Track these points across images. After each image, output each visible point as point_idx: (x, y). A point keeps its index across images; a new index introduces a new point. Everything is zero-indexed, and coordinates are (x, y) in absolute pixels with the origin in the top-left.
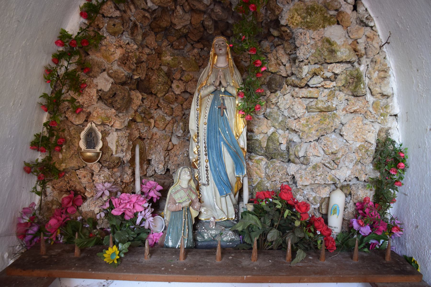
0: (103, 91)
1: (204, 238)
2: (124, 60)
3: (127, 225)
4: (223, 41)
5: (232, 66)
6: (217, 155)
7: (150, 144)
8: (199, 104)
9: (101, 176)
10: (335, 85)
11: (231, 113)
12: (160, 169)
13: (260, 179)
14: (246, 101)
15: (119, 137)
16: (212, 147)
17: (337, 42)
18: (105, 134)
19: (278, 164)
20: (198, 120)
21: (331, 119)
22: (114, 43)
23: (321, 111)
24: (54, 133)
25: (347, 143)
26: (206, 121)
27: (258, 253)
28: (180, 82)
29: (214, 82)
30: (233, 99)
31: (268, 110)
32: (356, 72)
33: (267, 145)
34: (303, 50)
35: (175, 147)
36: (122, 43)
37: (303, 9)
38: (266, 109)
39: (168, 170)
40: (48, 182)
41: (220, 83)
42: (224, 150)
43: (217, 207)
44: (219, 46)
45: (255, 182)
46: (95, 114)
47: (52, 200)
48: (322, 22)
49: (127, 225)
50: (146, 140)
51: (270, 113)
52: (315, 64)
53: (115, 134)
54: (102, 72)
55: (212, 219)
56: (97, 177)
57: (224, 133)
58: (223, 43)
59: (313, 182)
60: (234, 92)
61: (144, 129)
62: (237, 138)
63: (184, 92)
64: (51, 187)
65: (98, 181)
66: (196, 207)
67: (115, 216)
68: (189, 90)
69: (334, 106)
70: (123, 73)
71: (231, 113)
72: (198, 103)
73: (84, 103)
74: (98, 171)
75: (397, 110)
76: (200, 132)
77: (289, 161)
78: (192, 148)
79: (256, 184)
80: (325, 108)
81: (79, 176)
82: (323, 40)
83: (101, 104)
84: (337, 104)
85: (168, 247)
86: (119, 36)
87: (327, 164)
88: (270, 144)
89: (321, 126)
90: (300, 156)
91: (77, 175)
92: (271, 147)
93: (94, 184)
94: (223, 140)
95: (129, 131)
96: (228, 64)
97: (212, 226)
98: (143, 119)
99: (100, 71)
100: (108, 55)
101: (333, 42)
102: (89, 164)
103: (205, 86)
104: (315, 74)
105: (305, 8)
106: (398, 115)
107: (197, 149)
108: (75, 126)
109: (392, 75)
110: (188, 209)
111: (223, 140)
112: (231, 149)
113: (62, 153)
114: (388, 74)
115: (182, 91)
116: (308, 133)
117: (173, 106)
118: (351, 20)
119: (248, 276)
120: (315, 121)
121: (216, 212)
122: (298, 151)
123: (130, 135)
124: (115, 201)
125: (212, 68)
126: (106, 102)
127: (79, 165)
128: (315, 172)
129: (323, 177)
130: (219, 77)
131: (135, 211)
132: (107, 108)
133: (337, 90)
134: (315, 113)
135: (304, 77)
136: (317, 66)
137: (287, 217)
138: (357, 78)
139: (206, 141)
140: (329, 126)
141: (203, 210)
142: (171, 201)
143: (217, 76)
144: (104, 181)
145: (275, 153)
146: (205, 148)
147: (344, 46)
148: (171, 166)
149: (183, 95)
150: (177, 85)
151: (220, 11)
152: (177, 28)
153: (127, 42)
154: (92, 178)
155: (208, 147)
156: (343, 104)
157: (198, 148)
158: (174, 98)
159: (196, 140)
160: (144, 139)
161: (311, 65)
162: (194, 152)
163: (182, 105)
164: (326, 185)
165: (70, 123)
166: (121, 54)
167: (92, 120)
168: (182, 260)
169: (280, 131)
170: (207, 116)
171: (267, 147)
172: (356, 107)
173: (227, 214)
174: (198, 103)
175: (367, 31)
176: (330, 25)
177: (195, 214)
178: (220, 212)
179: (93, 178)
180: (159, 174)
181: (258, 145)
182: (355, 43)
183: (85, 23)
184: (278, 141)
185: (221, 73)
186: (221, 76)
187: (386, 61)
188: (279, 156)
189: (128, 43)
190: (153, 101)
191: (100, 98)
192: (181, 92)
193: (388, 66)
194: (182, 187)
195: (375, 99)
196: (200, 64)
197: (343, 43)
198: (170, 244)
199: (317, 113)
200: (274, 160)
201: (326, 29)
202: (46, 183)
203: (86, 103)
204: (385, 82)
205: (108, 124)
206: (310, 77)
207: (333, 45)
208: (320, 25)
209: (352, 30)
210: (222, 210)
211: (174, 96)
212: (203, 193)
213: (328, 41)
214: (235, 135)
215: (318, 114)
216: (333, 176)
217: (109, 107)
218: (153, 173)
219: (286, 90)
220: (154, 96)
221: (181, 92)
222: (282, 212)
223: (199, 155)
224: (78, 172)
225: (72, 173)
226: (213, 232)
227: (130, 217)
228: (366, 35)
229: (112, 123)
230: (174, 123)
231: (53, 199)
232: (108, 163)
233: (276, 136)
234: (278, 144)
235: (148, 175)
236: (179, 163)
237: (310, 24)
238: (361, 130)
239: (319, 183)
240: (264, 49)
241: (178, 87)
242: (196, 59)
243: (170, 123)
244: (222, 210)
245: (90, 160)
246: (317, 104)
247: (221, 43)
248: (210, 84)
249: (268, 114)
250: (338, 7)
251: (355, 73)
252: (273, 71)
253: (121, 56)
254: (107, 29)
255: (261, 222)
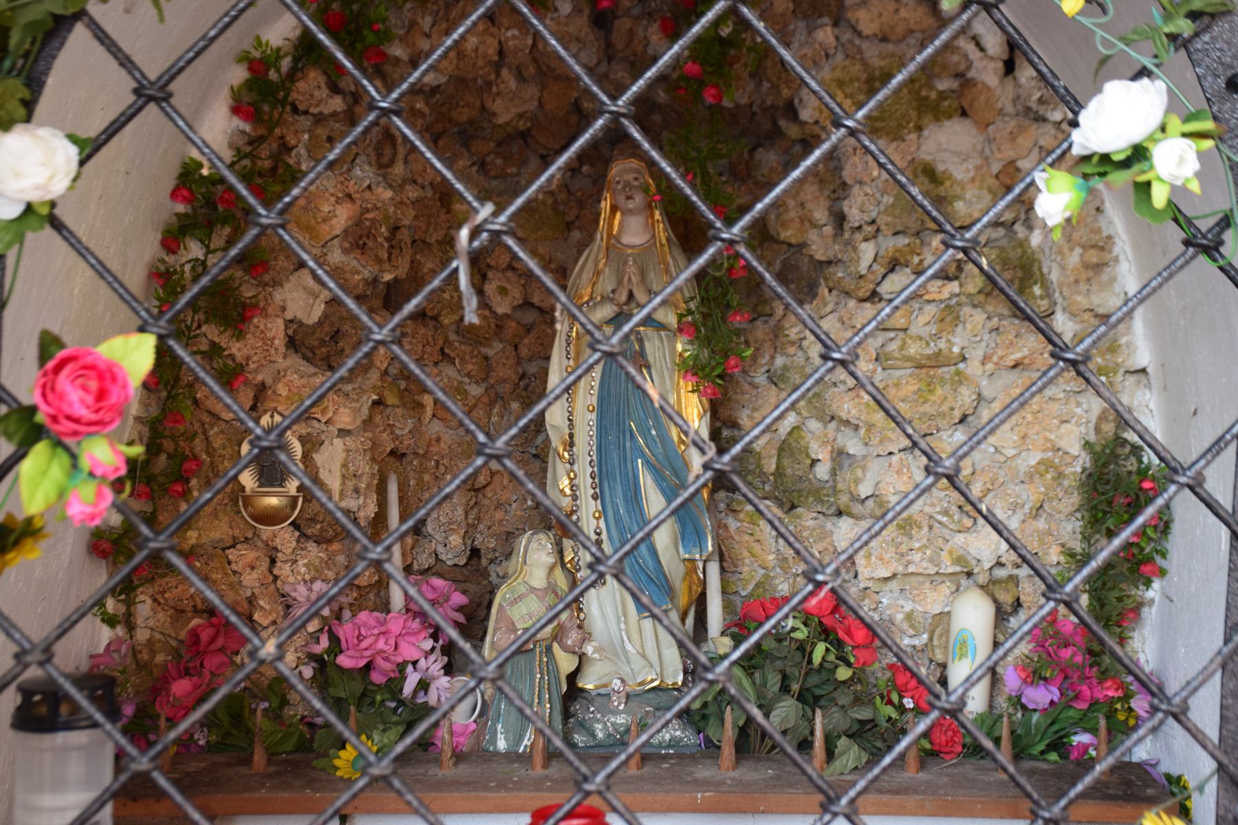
0: (301, 324)
1: (594, 736)
2: (361, 237)
3: (379, 698)
4: (638, 171)
5: (664, 241)
6: (625, 496)
7: (422, 470)
8: (572, 355)
9: (300, 563)
10: (957, 290)
11: (662, 377)
12: (452, 548)
13: (763, 571)
14: (706, 342)
15: (348, 451)
16: (611, 474)
17: (955, 173)
18: (311, 444)
19: (811, 523)
20: (571, 412)
21: (948, 387)
22: (332, 191)
23: (920, 367)
24: (161, 445)
25: (997, 456)
26: (594, 400)
27: (737, 752)
28: (510, 274)
29: (613, 291)
30: (667, 336)
31: (779, 361)
32: (1019, 251)
33: (778, 467)
34: (860, 199)
35: (495, 478)
36: (352, 187)
37: (858, 79)
38: (773, 357)
39: (475, 553)
40: (142, 585)
41: (631, 295)
42: (646, 481)
43: (627, 648)
44: (624, 188)
45: (748, 581)
46: (282, 390)
47: (149, 641)
48: (913, 114)
49: (379, 698)
50: (409, 458)
51: (785, 368)
52: (896, 234)
53: (338, 442)
54: (296, 270)
55: (617, 684)
56: (287, 567)
57: (645, 434)
58: (636, 179)
59: (900, 569)
60: (671, 319)
61: (405, 427)
62: (683, 447)
63: (520, 306)
64: (149, 601)
65: (291, 579)
66: (569, 642)
67: (347, 670)
68: (535, 300)
69: (956, 350)
70: (358, 273)
71: (662, 377)
72: (568, 353)
73: (248, 359)
74: (290, 550)
75: (1143, 356)
76: (577, 432)
77: (840, 514)
78: (556, 481)
79: (751, 587)
80: (929, 357)
81: (234, 566)
82: (916, 168)
83: (295, 361)
84: (966, 343)
85: (496, 753)
86: (345, 168)
87: (939, 517)
88: (786, 462)
89: (921, 409)
90: (863, 497)
91: (229, 563)
92: (789, 472)
93: (278, 589)
94: (643, 456)
95: (370, 435)
96: (654, 236)
97: (618, 703)
98: (401, 395)
99: (292, 267)
100: (313, 222)
101: (944, 172)
102: (266, 531)
103: (587, 302)
104: (893, 265)
105: (864, 76)
106: (1148, 370)
107: (571, 482)
108: (223, 425)
109: (1122, 257)
110: (549, 649)
111: (643, 456)
112: (664, 479)
113: (187, 501)
114: (1109, 256)
115: (515, 303)
116: (883, 429)
117: (490, 352)
118: (999, 105)
119: (707, 794)
120: (902, 394)
121: (628, 662)
122: (857, 481)
123: (375, 445)
124: (345, 631)
125: (607, 249)
126: (310, 355)
127: (237, 532)
128: (905, 539)
129: (928, 552)
130: (626, 279)
131: (400, 659)
132: (312, 370)
133: (966, 304)
134: (902, 372)
135: (863, 272)
136: (902, 241)
137: (821, 664)
138: (1023, 267)
139: (594, 458)
140: (945, 408)
141: (589, 649)
142: (501, 625)
143: (623, 277)
144: (307, 577)
145: (800, 491)
146: (593, 478)
147: (977, 184)
148: (486, 542)
149: (519, 314)
150: (499, 287)
151: (626, 75)
152: (500, 121)
153: (366, 184)
154: (271, 572)
155: (602, 476)
156: (984, 344)
157: (571, 480)
158: (493, 325)
159: (566, 454)
160: (404, 455)
161: (885, 236)
162: (562, 491)
163: (516, 347)
164: (936, 578)
165: (206, 414)
166: (350, 218)
167: (273, 405)
168: (539, 771)
169: (814, 425)
170: (596, 388)
171: (779, 473)
172: (1020, 350)
173: (659, 670)
174: (568, 353)
175: (1043, 135)
176: (937, 119)
177: (566, 664)
178: (637, 662)
179: (276, 572)
180: (449, 563)
181: (752, 467)
182: (1011, 170)
183: (243, 132)
184: (808, 455)
185: (632, 270)
186: (633, 278)
187: (1101, 218)
188: (811, 499)
189: (369, 187)
190: (430, 339)
191: (292, 343)
192: (514, 308)
193: (1105, 234)
194: (532, 588)
195: (1078, 327)
196: (571, 216)
197: (972, 174)
198: (502, 745)
199: (909, 371)
200: (800, 510)
201: (926, 133)
202: (134, 589)
203: (255, 359)
204: (1104, 277)
205: (318, 416)
206: (883, 271)
207: (942, 183)
208: (908, 123)
209: (998, 136)
210: (644, 656)
211: (492, 321)
212: (589, 608)
213: (930, 174)
214: (676, 439)
215: (911, 376)
216: (962, 552)
217: (316, 366)
218: (432, 561)
219: (825, 305)
220: (431, 323)
221: (514, 308)
222: (808, 649)
223: (575, 498)
224: (232, 554)
225: (211, 557)
226: (621, 720)
227: (385, 675)
228: (1041, 148)
229: (330, 414)
230: (491, 404)
231: (152, 636)
232: (318, 526)
233: (803, 438)
234: (808, 462)
235: (416, 567)
236: (510, 529)
237: (878, 124)
238: (1040, 415)
239: (921, 571)
240: (763, 176)
241: (503, 291)
242: (556, 201)
243: (481, 405)
244: (644, 656)
245: (270, 518)
246: (903, 347)
247: (630, 177)
248: (602, 297)
249: (779, 372)
250: (962, 67)
251: (1014, 254)
252: (794, 241)
253: (350, 223)
254: (309, 151)
255: (754, 683)
